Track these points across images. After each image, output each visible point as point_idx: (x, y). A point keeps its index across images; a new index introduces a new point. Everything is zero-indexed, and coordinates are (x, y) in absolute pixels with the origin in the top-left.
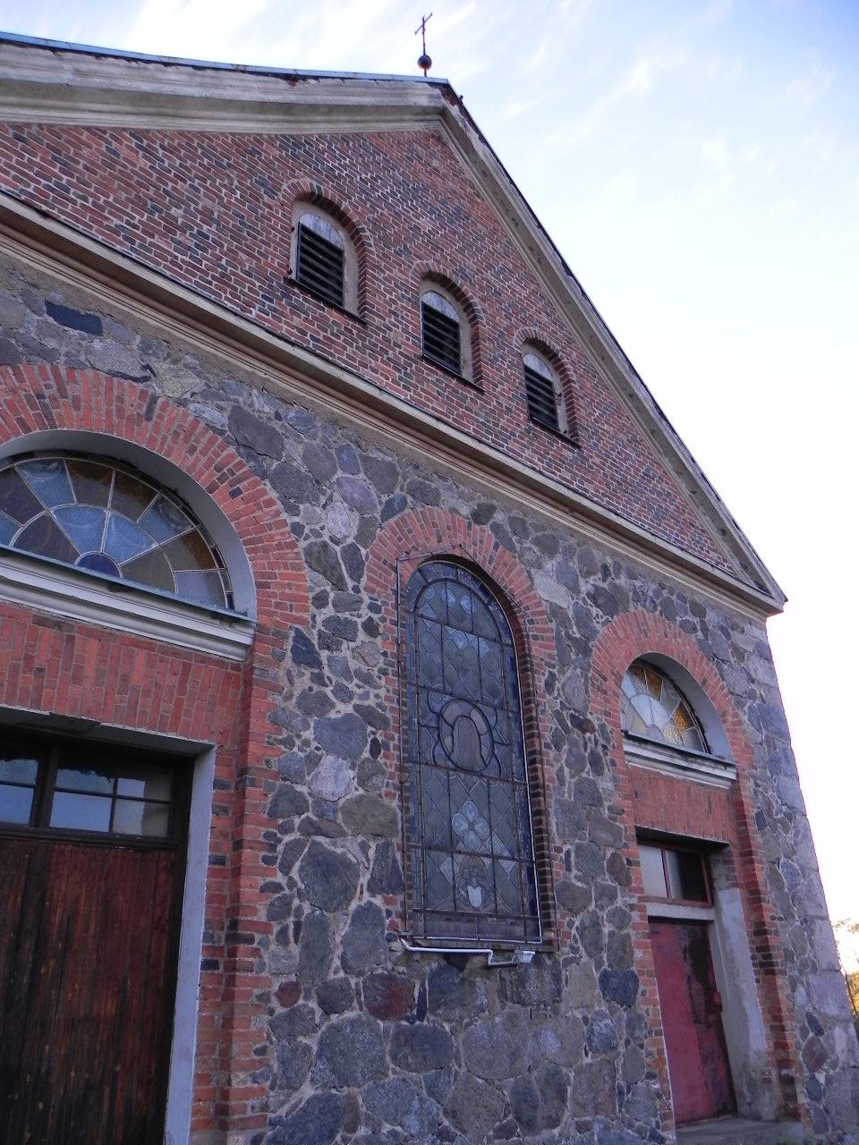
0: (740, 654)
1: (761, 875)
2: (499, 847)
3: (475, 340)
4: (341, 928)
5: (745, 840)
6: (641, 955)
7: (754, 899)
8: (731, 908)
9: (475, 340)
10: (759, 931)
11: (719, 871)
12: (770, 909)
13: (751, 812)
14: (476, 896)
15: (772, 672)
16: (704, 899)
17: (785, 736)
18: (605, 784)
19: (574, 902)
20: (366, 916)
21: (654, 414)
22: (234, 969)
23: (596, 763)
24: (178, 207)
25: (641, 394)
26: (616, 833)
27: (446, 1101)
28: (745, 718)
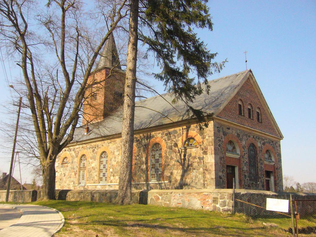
0: (277, 147)
1: (276, 175)
2: (255, 173)
3: (252, 111)
4: (246, 180)
5: (275, 170)
6: (265, 183)
7: (275, 178)
8: (272, 178)
9: (252, 111)
10: (275, 181)
11: (271, 175)
12: (277, 178)
13: (276, 168)
14: (253, 178)
15: (280, 148)
16: (269, 177)
17: (281, 157)
18: (263, 166)
19: (260, 178)
20: (247, 179)
21: (270, 114)
22: (66, 95)
23: (262, 164)
24: (190, 42)
25: (269, 111)
26: (263, 171)
27: (209, 179)
28: (276, 156)
